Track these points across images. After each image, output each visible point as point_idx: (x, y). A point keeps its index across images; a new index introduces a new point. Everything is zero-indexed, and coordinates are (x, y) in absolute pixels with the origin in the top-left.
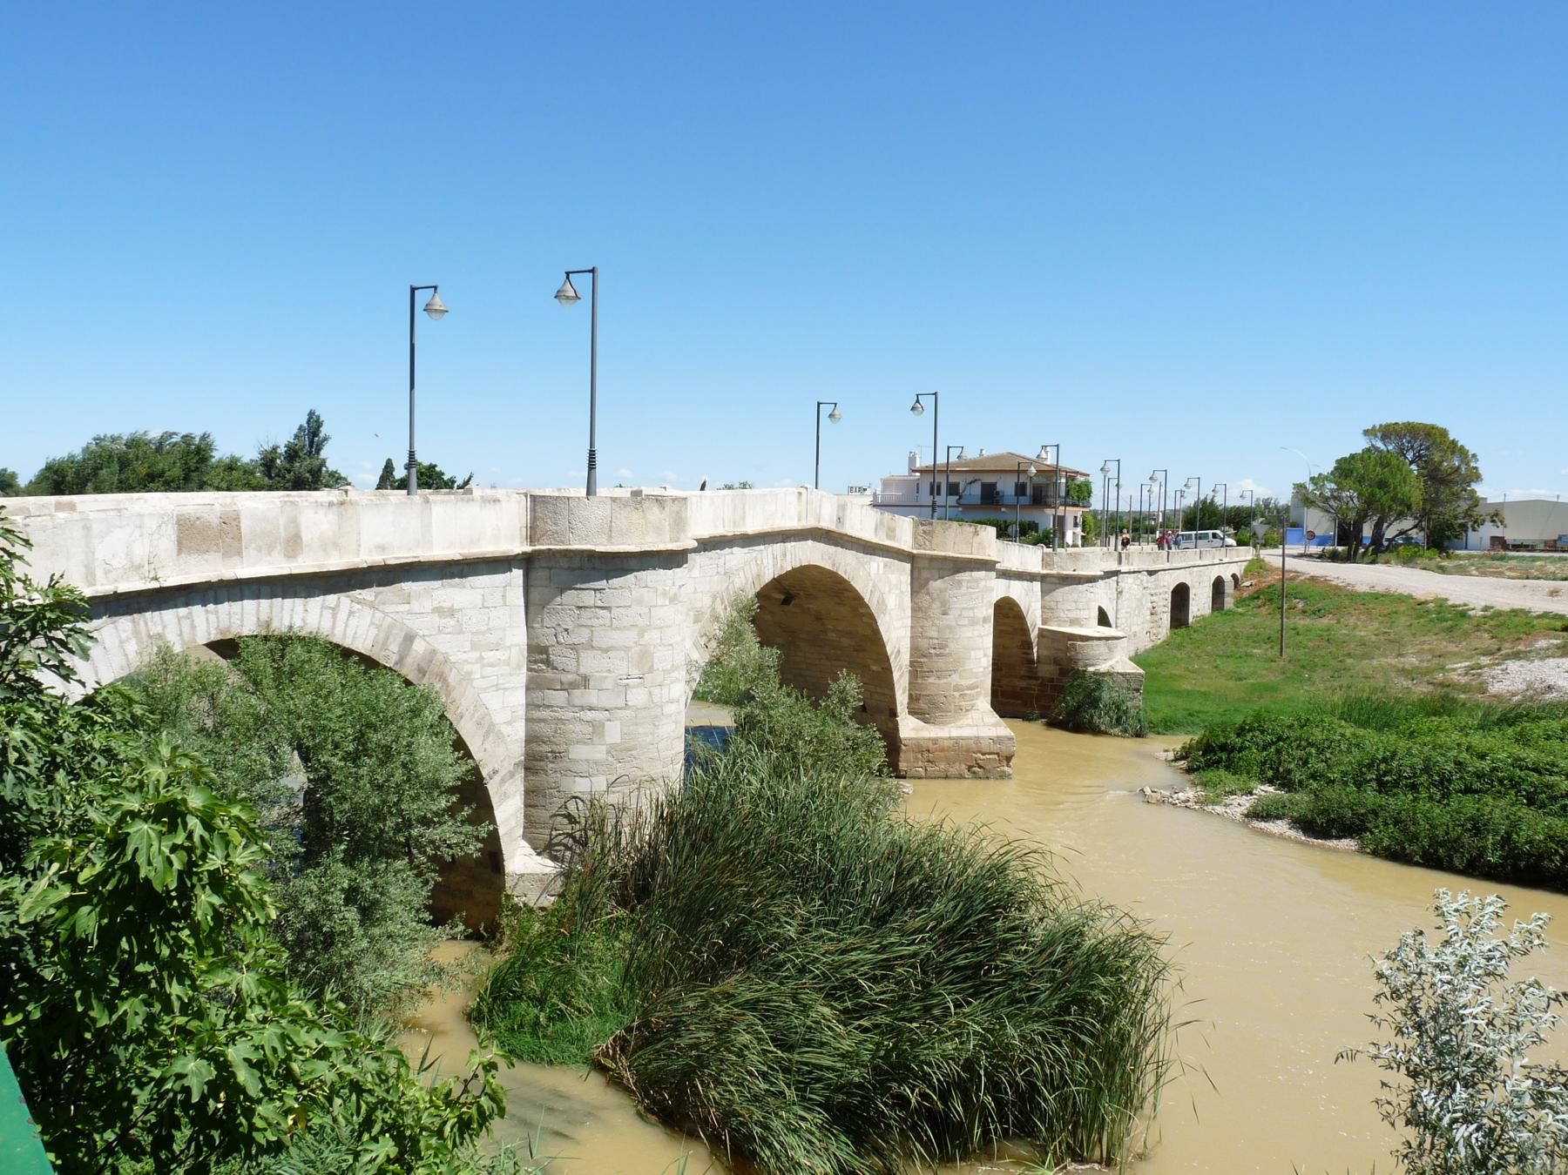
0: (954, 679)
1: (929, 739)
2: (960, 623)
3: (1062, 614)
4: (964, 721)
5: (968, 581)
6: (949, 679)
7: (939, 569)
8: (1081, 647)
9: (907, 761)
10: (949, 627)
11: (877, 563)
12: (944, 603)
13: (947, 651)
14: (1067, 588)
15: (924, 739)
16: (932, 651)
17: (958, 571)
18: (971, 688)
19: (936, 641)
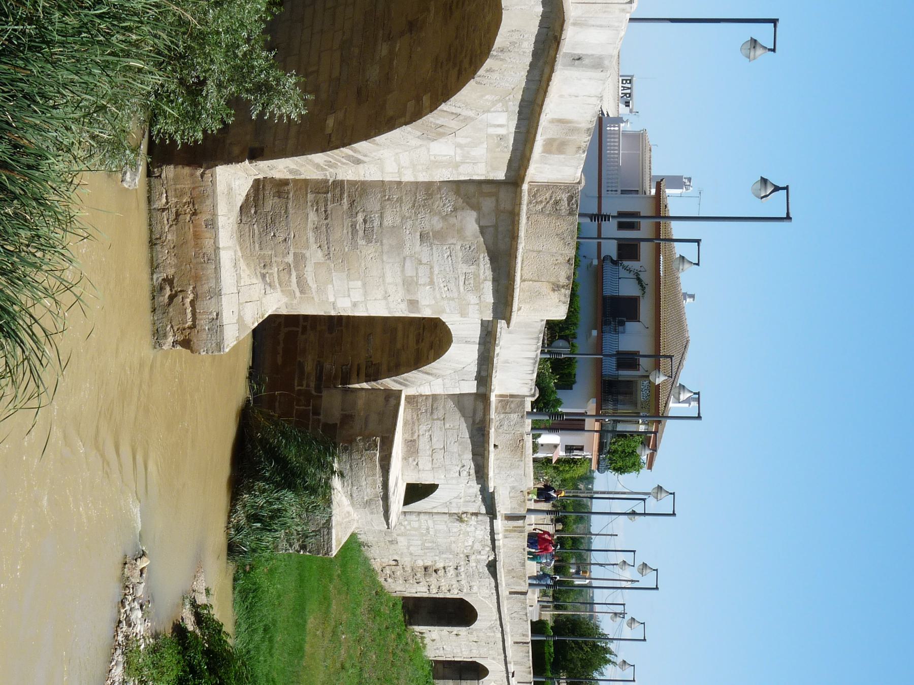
0: (315, 255)
1: (214, 215)
2: (408, 264)
3: (423, 428)
4: (246, 272)
5: (476, 276)
6: (314, 247)
7: (496, 227)
8: (372, 459)
9: (176, 179)
10: (400, 246)
13: (362, 242)
14: (467, 436)
15: (214, 206)
16: (360, 218)
17: (494, 258)
19: (376, 223)
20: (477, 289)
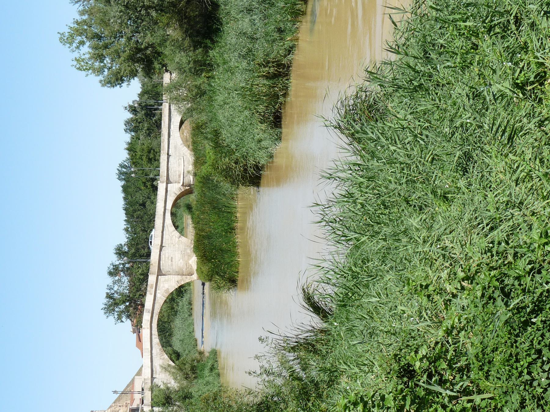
0: (184, 270)
11: (158, 295)
18: (186, 265)
20: (163, 264)
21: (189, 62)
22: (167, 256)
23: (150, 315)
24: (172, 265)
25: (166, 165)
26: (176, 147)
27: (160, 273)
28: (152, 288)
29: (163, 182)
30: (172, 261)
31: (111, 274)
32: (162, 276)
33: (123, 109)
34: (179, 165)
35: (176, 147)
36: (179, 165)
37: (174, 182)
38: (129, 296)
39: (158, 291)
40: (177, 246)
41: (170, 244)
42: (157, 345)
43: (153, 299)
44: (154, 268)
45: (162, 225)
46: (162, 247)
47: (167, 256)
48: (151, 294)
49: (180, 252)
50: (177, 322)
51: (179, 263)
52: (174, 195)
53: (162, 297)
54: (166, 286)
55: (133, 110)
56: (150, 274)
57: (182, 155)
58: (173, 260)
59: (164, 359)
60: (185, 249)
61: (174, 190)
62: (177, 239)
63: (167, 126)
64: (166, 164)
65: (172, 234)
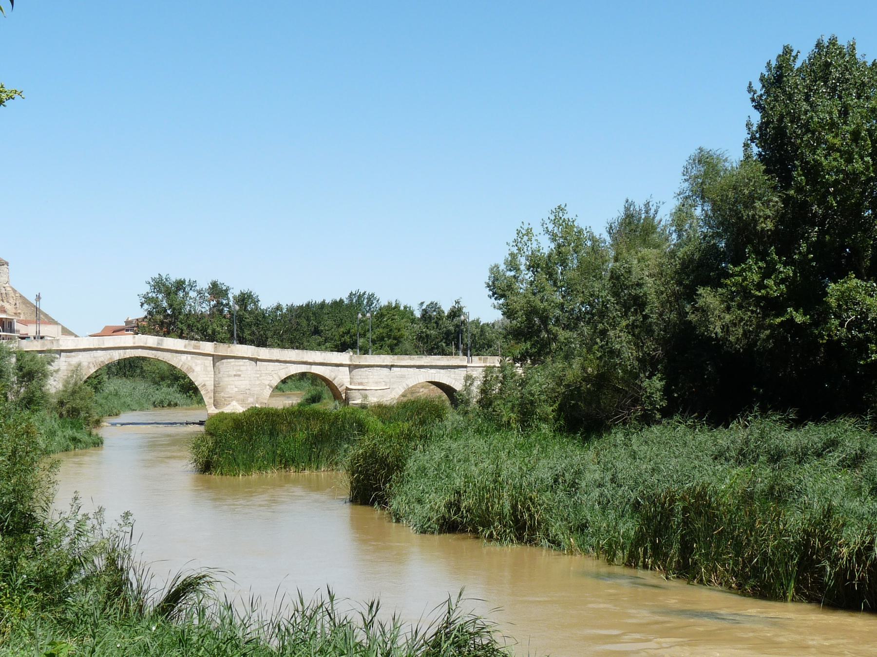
0: (222, 394)
12: (219, 370)
20: (230, 362)
21: (533, 395)
22: (242, 368)
23: (155, 346)
24: (229, 376)
25: (376, 364)
26: (403, 377)
27: (217, 359)
28: (195, 347)
29: (351, 360)
30: (235, 375)
31: (215, 285)
32: (212, 362)
33: (456, 299)
34: (376, 383)
35: (403, 377)
36: (376, 383)
37: (352, 377)
38: (180, 313)
39: (189, 356)
40: (258, 382)
41: (259, 372)
42: (109, 357)
43: (178, 349)
44: (224, 349)
45: (288, 359)
46: (256, 360)
47: (242, 368)
48: (185, 347)
49: (248, 387)
50: (141, 386)
51: (232, 387)
52: (333, 377)
53: (181, 363)
54: (198, 369)
55: (456, 313)
56: (215, 344)
57: (391, 387)
58: (236, 378)
59: (89, 367)
60: (252, 395)
61: (340, 377)
62: (267, 382)
63: (434, 364)
64: (378, 364)
65: (274, 375)
